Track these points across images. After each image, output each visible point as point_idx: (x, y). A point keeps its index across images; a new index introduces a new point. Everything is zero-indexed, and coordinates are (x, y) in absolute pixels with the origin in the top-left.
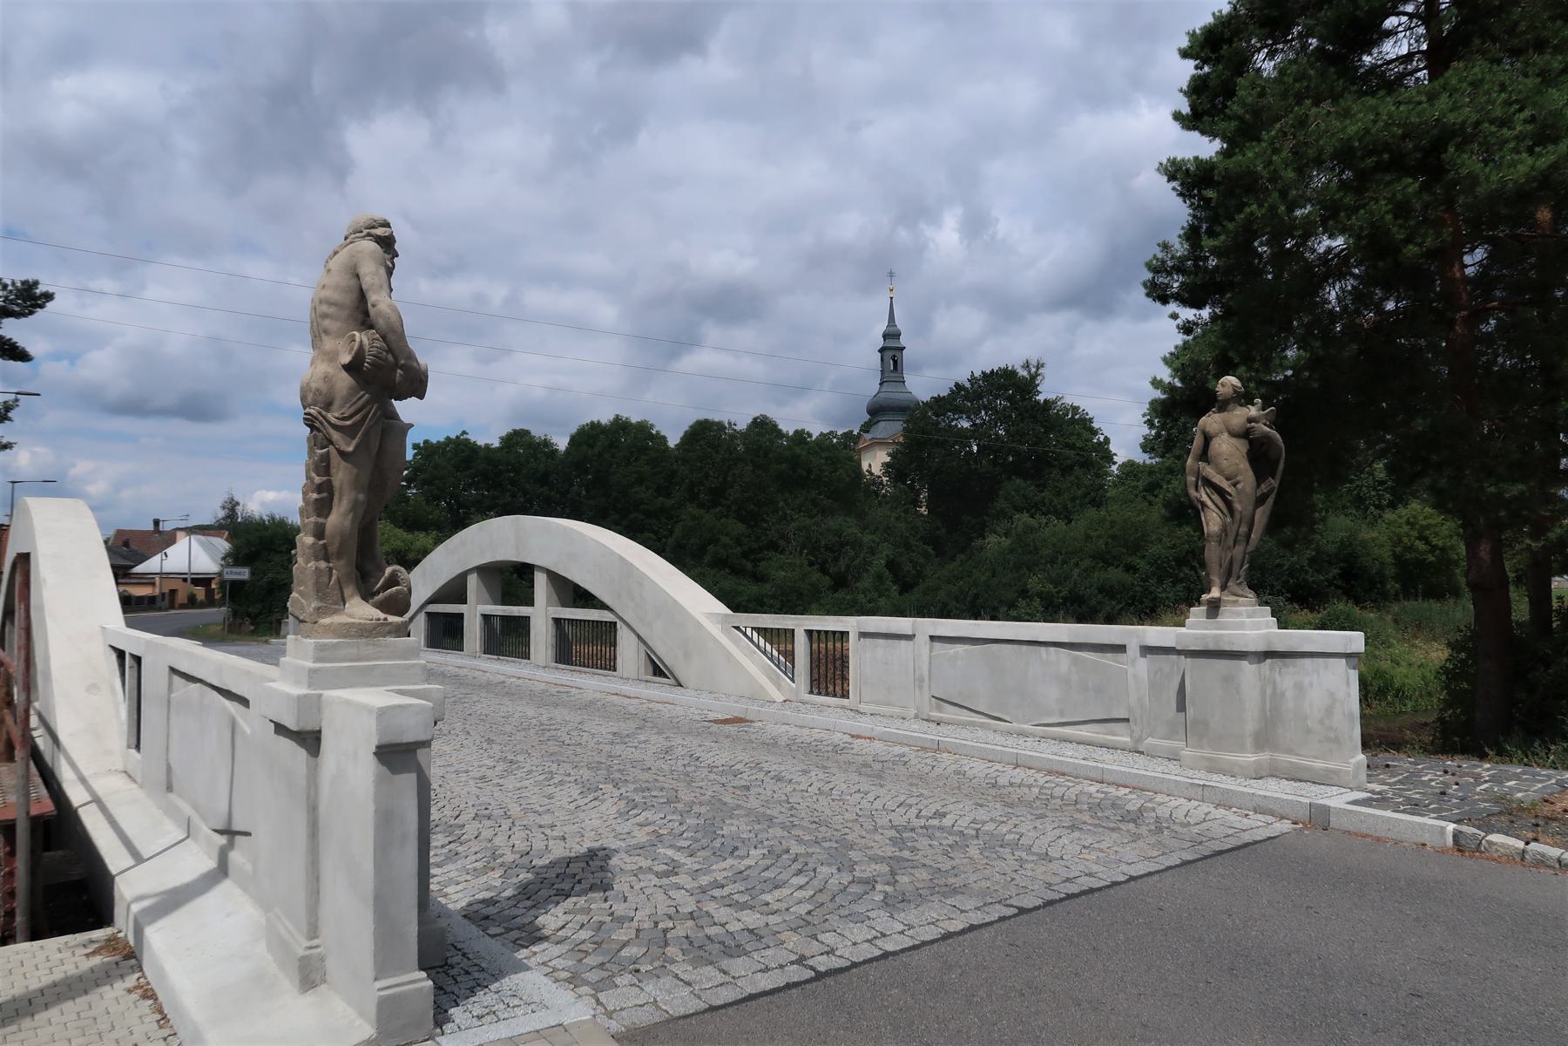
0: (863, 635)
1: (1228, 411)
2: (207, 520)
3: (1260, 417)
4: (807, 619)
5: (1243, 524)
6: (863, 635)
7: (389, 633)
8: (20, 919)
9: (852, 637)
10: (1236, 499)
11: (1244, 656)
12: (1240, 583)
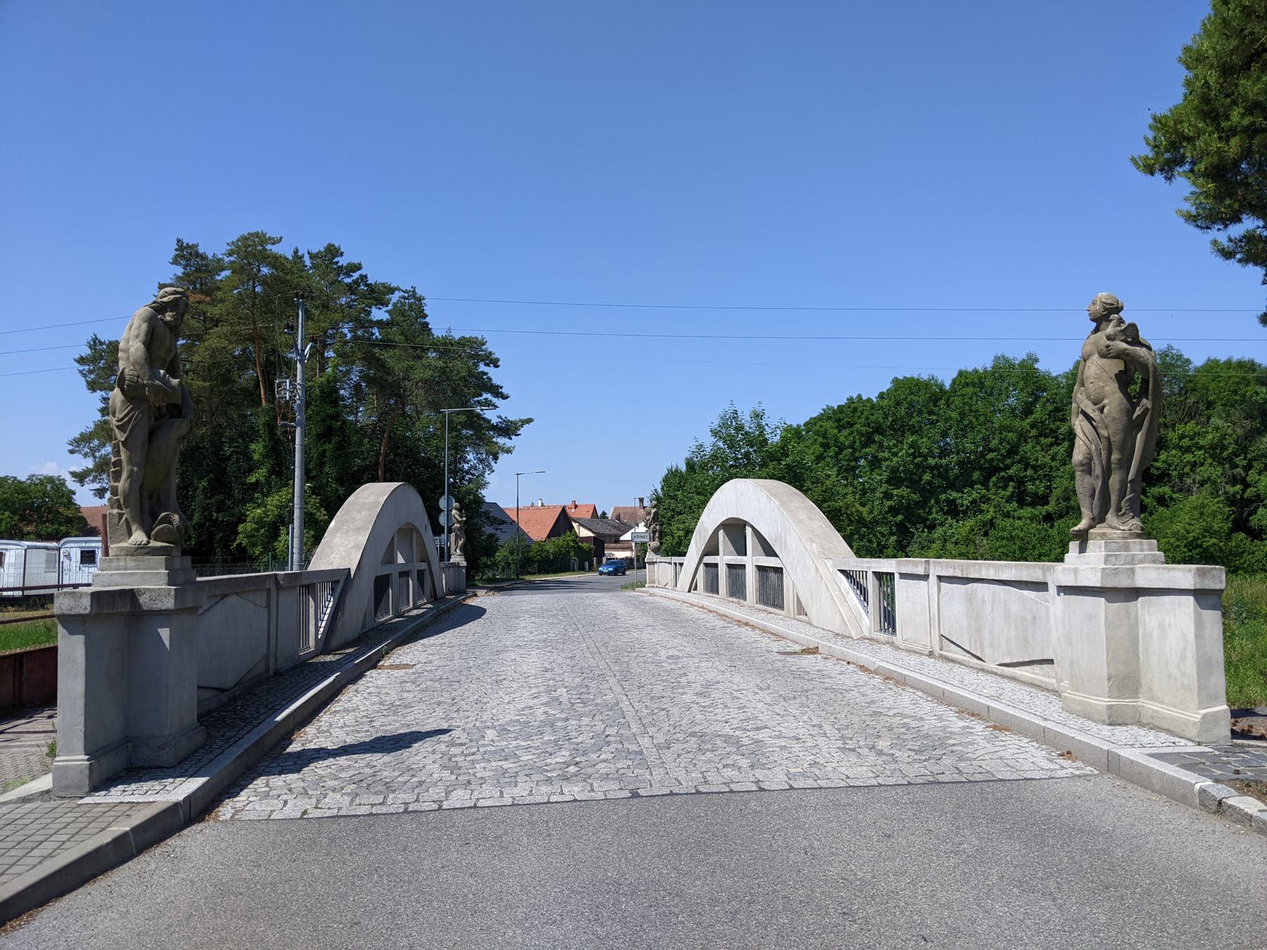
0: (904, 576)
1: (1102, 330)
2: (526, 426)
3: (1115, 335)
4: (1005, 565)
5: (1114, 451)
6: (904, 576)
7: (147, 554)
8: (132, 838)
9: (897, 576)
10: (1100, 425)
11: (1103, 592)
12: (1123, 515)
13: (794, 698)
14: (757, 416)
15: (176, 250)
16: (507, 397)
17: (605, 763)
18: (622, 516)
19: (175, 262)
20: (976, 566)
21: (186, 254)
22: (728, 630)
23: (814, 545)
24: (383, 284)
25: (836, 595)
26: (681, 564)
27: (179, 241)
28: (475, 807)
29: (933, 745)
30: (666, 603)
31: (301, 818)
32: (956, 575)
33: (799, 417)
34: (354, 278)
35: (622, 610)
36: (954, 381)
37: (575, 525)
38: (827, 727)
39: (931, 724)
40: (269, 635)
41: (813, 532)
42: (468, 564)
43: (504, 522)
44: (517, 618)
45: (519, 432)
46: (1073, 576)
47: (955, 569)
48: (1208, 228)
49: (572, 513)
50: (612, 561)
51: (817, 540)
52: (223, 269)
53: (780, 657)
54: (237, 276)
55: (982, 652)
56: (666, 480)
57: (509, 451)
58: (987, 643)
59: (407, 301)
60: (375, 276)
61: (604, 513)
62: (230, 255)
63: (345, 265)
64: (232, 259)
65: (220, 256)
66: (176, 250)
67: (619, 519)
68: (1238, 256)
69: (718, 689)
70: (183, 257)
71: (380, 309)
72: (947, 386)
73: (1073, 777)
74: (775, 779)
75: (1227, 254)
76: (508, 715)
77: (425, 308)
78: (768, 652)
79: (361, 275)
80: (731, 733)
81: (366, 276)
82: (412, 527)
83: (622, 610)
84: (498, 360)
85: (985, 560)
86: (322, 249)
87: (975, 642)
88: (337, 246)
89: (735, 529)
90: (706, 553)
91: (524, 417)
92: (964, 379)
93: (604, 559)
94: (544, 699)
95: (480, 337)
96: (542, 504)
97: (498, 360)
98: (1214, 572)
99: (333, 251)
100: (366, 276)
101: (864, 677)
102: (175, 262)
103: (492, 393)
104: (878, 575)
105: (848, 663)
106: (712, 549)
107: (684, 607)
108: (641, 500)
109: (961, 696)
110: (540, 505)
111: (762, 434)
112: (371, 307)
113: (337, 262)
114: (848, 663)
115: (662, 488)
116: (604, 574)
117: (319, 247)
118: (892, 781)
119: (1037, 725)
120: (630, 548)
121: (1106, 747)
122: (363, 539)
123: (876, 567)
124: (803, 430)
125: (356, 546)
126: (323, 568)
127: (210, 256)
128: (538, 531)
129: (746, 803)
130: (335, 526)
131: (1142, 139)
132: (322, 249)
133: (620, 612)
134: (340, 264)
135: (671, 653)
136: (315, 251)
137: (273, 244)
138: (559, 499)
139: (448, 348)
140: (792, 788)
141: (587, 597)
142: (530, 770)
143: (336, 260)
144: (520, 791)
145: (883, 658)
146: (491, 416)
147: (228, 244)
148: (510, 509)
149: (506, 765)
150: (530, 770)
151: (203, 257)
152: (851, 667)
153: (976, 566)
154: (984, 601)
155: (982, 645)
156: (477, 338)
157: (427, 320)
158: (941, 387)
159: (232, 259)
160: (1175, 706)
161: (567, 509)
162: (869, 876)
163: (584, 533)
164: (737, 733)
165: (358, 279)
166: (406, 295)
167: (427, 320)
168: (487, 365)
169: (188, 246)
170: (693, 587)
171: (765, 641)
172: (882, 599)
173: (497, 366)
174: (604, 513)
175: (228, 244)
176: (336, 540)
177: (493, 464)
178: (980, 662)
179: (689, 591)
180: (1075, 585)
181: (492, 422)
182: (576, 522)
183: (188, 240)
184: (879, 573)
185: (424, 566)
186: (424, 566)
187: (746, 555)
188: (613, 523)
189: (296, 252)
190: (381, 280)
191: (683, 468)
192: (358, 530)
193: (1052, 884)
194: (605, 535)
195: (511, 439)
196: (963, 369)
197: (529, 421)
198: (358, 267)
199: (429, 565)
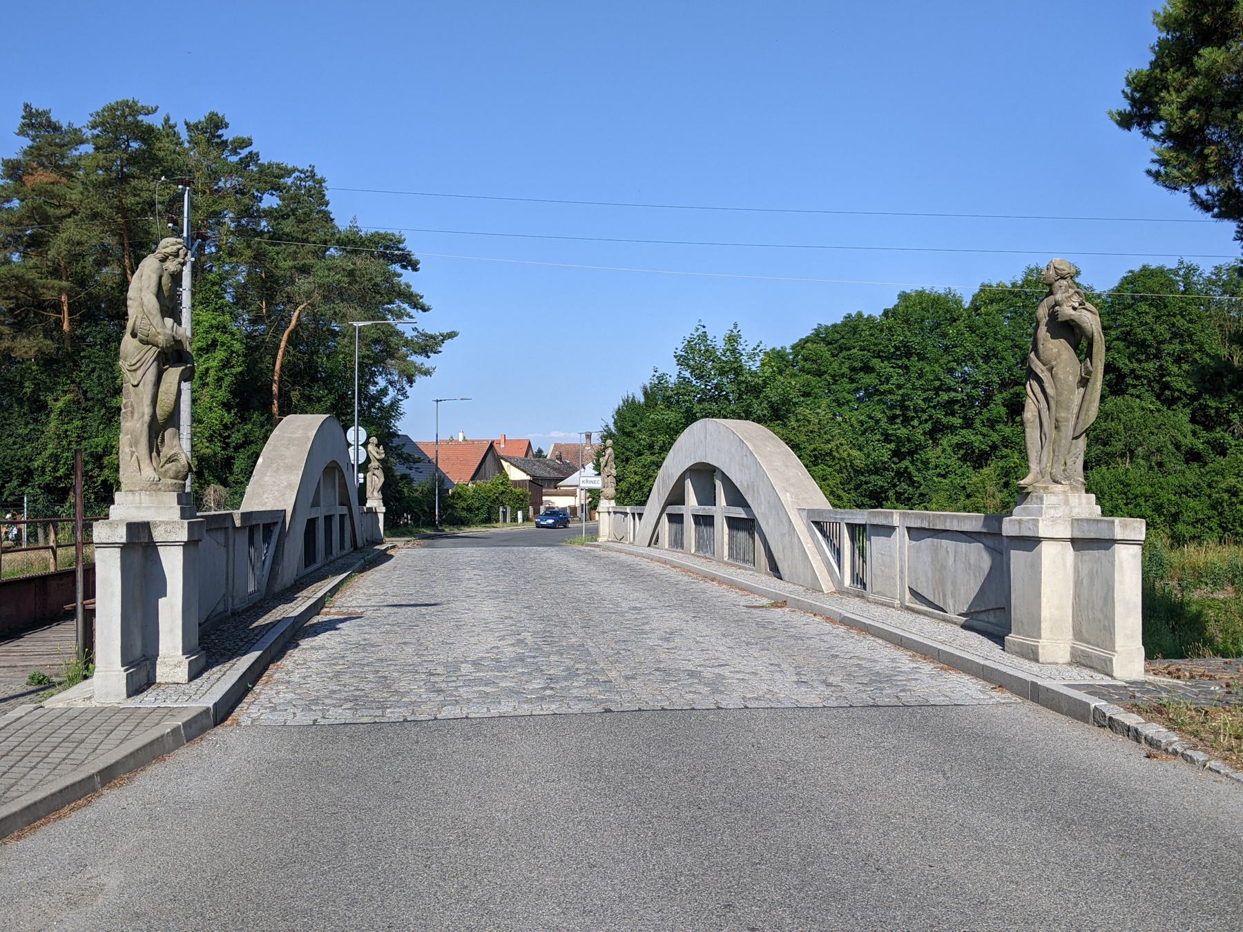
13: (756, 644)
14: (732, 339)
15: (24, 118)
16: (428, 310)
17: (577, 687)
18: (563, 456)
19: (22, 133)
20: (942, 518)
21: (35, 122)
22: (693, 585)
23: (788, 494)
24: (278, 165)
25: (808, 548)
26: (640, 515)
27: (27, 106)
28: (467, 718)
29: (879, 679)
30: (623, 557)
31: (314, 724)
32: (923, 526)
33: (786, 340)
34: (242, 156)
35: (573, 564)
36: (975, 298)
37: (505, 464)
38: (785, 666)
39: (883, 665)
40: (227, 574)
41: (788, 480)
42: (386, 509)
43: (418, 461)
44: (458, 569)
45: (440, 349)
46: (1017, 526)
47: (922, 520)
48: (1175, 189)
49: (501, 449)
50: (552, 512)
51: (792, 490)
52: (82, 142)
53: (745, 610)
54: (101, 156)
55: (945, 602)
56: (619, 412)
57: (427, 373)
58: (949, 593)
59: (303, 183)
60: (269, 154)
61: (540, 451)
62: (94, 127)
63: (230, 139)
64: (96, 132)
65: (76, 126)
66: (24, 118)
67: (560, 459)
68: (1216, 210)
69: (682, 635)
70: (31, 126)
71: (272, 195)
72: (967, 303)
73: (999, 703)
74: (731, 701)
75: (1206, 207)
76: (477, 652)
77: (326, 192)
78: (735, 605)
79: (250, 153)
80: (694, 669)
81: (257, 154)
82: (334, 465)
83: (573, 564)
84: (417, 262)
85: (969, 512)
86: (203, 119)
87: (939, 593)
88: (220, 115)
89: (704, 474)
90: (669, 502)
91: (445, 331)
92: (990, 297)
93: (542, 510)
94: (510, 640)
95: (397, 233)
96: (464, 438)
97: (417, 262)
98: (1135, 524)
99: (216, 123)
100: (257, 154)
101: (828, 627)
102: (22, 133)
103: (410, 304)
104: (852, 527)
105: (815, 615)
106: (677, 497)
107: (644, 563)
108: (589, 436)
109: (917, 642)
110: (461, 439)
111: (737, 360)
112: (263, 194)
113: (220, 137)
114: (815, 615)
115: (615, 423)
116: (543, 526)
117: (198, 116)
118: (835, 704)
119: (977, 663)
120: (573, 494)
121: (1030, 678)
122: (296, 478)
123: (849, 519)
124: (790, 354)
125: (289, 486)
126: (255, 509)
127: (65, 127)
128: (459, 475)
129: (705, 717)
130: (263, 462)
131: (1121, 93)
132: (203, 119)
133: (571, 566)
134: (224, 138)
135: (633, 604)
136: (192, 121)
137: (146, 114)
138: (485, 433)
139: (353, 244)
140: (746, 707)
141: (518, 551)
142: (511, 692)
143: (220, 132)
144: (507, 707)
145: (852, 608)
146: (406, 328)
147: (91, 115)
148: (427, 444)
149: (488, 689)
150: (511, 692)
151: (56, 128)
152: (818, 619)
153: (942, 518)
154: (947, 552)
155: (944, 596)
156: (393, 235)
157: (329, 208)
158: (958, 302)
159: (96, 132)
160: (1098, 646)
161: (494, 444)
162: (802, 760)
163: (515, 474)
164: (699, 669)
165: (246, 157)
166: (302, 176)
167: (329, 208)
168: (404, 267)
169: (38, 114)
170: (654, 540)
171: (733, 595)
172: (857, 556)
173: (415, 269)
174: (540, 451)
175: (91, 115)
176: (267, 479)
177: (407, 387)
178: (942, 613)
179: (649, 545)
180: (1018, 535)
181: (406, 335)
182: (506, 461)
183: (38, 105)
184: (852, 524)
185: (345, 510)
186: (345, 510)
187: (715, 505)
188: (552, 463)
189: (167, 120)
190: (275, 160)
191: (641, 399)
192: (290, 468)
193: (947, 767)
194: (544, 479)
195: (429, 357)
196: (986, 282)
197: (451, 335)
198: (248, 143)
199: (350, 509)
